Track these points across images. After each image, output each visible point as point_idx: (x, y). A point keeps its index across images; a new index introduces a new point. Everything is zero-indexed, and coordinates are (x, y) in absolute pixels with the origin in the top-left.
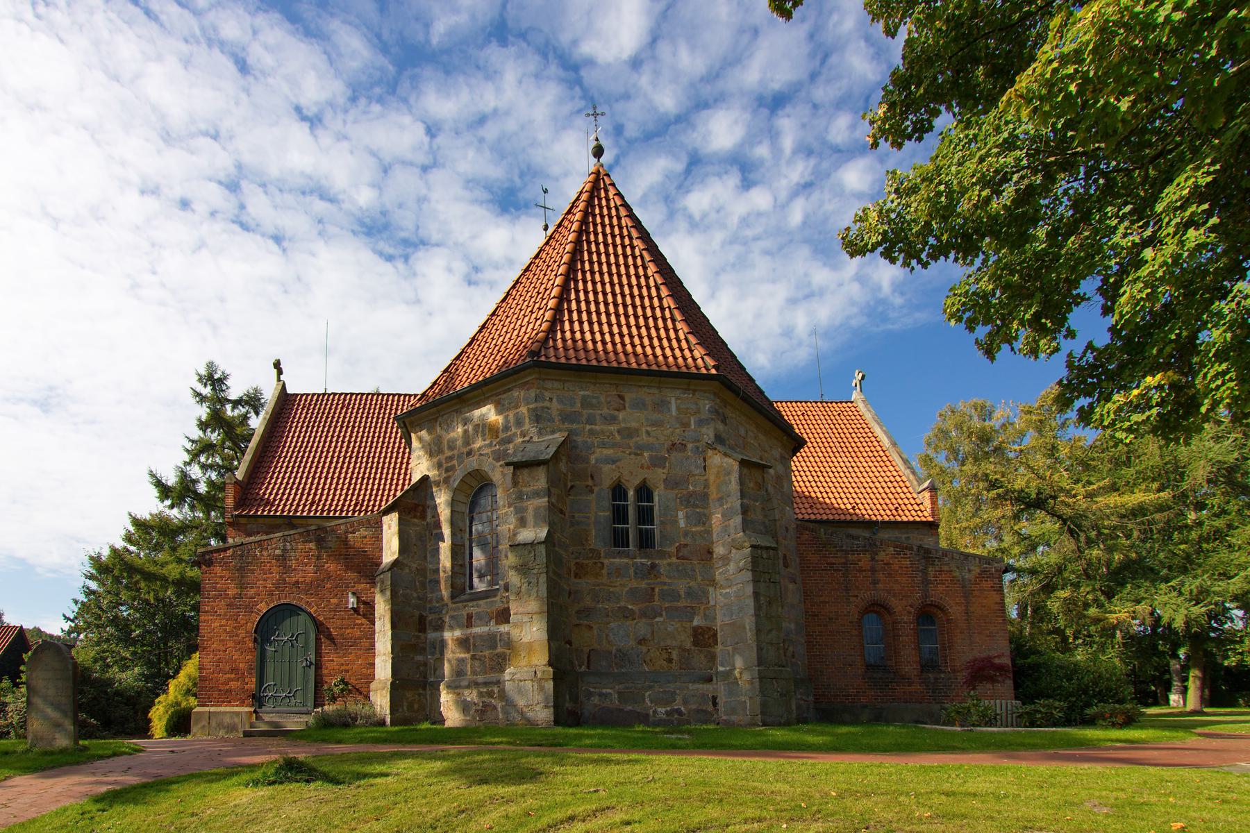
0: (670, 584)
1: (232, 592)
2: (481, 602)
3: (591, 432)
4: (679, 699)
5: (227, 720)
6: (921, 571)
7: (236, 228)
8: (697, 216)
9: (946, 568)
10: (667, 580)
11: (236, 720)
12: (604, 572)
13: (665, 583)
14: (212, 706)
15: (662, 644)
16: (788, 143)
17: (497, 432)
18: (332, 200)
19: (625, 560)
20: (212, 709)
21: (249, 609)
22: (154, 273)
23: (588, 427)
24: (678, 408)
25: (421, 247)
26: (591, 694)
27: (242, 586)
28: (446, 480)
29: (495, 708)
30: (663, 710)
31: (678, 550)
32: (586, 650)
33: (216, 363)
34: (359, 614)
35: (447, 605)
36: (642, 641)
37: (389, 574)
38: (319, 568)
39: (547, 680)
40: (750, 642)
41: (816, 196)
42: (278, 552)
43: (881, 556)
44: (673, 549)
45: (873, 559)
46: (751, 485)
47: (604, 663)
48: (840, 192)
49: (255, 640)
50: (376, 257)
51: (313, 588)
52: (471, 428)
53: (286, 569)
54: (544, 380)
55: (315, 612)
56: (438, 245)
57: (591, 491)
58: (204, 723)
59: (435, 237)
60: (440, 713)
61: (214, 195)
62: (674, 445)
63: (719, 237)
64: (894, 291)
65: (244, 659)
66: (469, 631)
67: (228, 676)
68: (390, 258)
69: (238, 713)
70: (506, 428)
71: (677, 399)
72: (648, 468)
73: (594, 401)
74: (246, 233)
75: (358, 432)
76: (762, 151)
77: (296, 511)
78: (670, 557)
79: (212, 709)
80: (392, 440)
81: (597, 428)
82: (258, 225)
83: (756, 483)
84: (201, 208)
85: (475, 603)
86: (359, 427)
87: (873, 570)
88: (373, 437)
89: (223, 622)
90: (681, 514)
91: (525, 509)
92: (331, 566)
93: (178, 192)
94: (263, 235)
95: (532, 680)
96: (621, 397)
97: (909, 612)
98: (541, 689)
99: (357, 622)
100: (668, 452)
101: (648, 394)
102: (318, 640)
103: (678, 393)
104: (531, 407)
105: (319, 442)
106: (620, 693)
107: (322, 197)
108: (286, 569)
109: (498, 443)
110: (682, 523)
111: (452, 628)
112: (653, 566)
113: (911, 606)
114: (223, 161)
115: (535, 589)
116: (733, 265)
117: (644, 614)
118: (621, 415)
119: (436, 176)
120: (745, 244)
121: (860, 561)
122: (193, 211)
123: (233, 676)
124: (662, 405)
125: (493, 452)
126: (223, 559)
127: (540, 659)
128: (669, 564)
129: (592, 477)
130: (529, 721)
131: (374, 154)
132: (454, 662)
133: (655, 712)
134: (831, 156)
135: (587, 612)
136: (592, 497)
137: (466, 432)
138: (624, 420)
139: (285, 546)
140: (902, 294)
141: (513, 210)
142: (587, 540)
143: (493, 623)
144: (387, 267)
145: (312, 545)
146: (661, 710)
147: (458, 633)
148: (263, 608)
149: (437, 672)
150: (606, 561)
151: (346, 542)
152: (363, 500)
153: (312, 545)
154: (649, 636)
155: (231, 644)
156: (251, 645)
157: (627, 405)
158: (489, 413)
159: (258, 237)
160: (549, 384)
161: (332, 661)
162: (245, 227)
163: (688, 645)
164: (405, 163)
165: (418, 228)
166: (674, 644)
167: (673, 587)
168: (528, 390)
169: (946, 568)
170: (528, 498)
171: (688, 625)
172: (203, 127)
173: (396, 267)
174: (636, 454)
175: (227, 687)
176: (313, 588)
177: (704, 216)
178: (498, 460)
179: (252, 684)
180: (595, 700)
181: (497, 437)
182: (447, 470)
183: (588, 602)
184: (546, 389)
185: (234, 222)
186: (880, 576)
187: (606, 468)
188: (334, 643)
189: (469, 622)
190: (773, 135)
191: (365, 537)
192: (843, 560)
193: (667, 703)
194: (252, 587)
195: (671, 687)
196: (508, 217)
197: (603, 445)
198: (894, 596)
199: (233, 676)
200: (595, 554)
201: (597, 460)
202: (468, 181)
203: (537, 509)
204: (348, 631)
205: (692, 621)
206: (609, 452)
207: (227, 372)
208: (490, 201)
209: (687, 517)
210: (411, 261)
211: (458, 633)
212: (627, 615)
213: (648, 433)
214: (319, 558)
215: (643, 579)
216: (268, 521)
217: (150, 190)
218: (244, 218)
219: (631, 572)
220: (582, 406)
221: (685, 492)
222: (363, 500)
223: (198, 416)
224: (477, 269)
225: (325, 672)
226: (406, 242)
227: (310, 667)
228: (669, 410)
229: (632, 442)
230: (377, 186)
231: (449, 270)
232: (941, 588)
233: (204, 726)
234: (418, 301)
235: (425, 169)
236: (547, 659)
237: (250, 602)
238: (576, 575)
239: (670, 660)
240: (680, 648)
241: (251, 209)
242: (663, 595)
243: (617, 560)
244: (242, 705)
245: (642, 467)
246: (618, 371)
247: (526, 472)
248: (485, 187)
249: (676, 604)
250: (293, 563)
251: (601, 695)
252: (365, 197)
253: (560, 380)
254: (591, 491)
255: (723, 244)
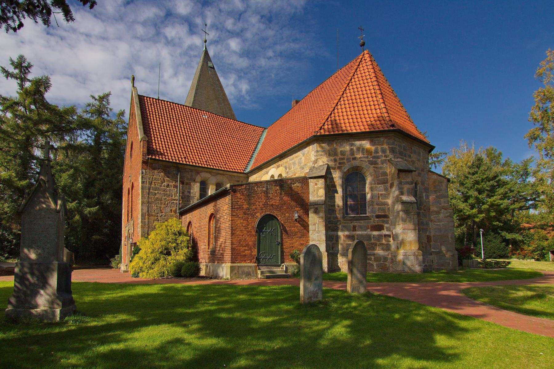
1: (245, 207)
2: (362, 221)
5: (246, 270)
8: (169, 39)
11: (250, 270)
14: (238, 263)
16: (209, 22)
17: (371, 152)
20: (239, 264)
21: (253, 216)
27: (249, 204)
28: (339, 168)
29: (373, 265)
33: (26, 57)
34: (297, 222)
35: (340, 221)
37: (324, 206)
38: (281, 199)
39: (420, 256)
40: (450, 242)
41: (219, 47)
42: (264, 189)
48: (228, 47)
49: (257, 232)
51: (279, 208)
52: (355, 148)
53: (268, 198)
55: (280, 219)
58: (236, 271)
60: (338, 266)
63: (179, 51)
64: (247, 94)
65: (252, 240)
66: (354, 233)
67: (244, 248)
69: (251, 267)
70: (376, 151)
76: (198, 21)
79: (239, 264)
85: (358, 221)
89: (242, 221)
91: (403, 188)
92: (285, 198)
95: (414, 256)
98: (417, 259)
99: (296, 225)
104: (390, 146)
108: (268, 198)
109: (372, 157)
111: (342, 231)
115: (413, 220)
116: (185, 65)
120: (190, 57)
123: (246, 248)
125: (368, 161)
126: (240, 190)
127: (415, 247)
130: (413, 271)
132: (345, 245)
134: (225, 33)
137: (352, 149)
139: (267, 187)
140: (250, 96)
143: (368, 230)
145: (278, 188)
147: (347, 233)
149: (334, 249)
151: (291, 188)
153: (278, 188)
155: (245, 232)
156: (254, 233)
158: (366, 144)
161: (287, 242)
168: (389, 139)
170: (404, 184)
175: (244, 254)
176: (279, 208)
177: (172, 40)
178: (371, 164)
179: (255, 252)
181: (371, 155)
182: (340, 163)
188: (287, 234)
189: (354, 229)
190: (203, 16)
191: (298, 187)
194: (254, 205)
199: (246, 248)
203: (408, 189)
204: (292, 229)
207: (32, 64)
211: (347, 233)
214: (281, 194)
216: (164, 163)
225: (284, 247)
227: (279, 245)
233: (236, 273)
236: (418, 247)
237: (253, 212)
244: (251, 262)
247: (403, 174)
250: (271, 195)
253: (399, 138)
255: (180, 55)
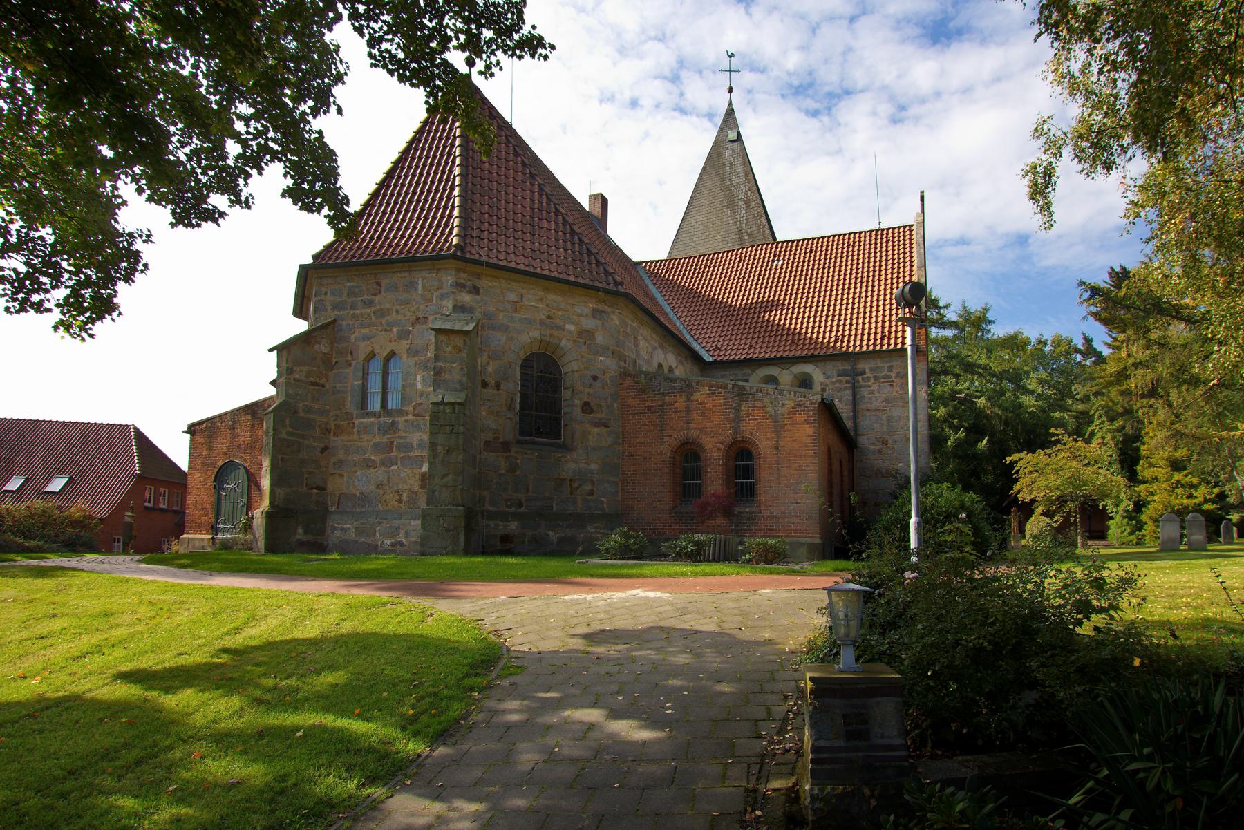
0: (406, 437)
3: (354, 316)
4: (402, 533)
6: (734, 408)
7: (676, 114)
9: (759, 404)
10: (404, 434)
12: (355, 430)
13: (401, 437)
15: (395, 488)
18: (763, 71)
19: (372, 420)
20: (191, 536)
21: (214, 464)
22: (608, 169)
23: (352, 312)
24: (424, 287)
25: (845, 97)
26: (335, 528)
27: (210, 449)
30: (389, 542)
31: (414, 409)
32: (338, 494)
36: (379, 486)
43: (697, 396)
44: (411, 409)
45: (688, 400)
46: (449, 349)
47: (350, 504)
49: (215, 487)
50: (802, 116)
54: (321, 278)
56: (862, 91)
57: (350, 365)
59: (860, 85)
61: (657, 90)
62: (418, 319)
68: (815, 114)
69: (203, 539)
71: (424, 278)
72: (395, 341)
73: (357, 290)
74: (685, 118)
75: (823, 273)
77: (875, 345)
78: (407, 415)
79: (191, 536)
80: (819, 280)
81: (358, 312)
82: (694, 108)
83: (455, 347)
84: (646, 102)
86: (835, 267)
87: (688, 410)
88: (788, 285)
90: (419, 378)
93: (627, 95)
94: (698, 116)
96: (379, 284)
97: (719, 449)
100: (413, 325)
101: (400, 278)
102: (249, 486)
103: (424, 274)
105: (781, 291)
106: (356, 528)
107: (752, 70)
110: (419, 386)
112: (393, 423)
113: (722, 443)
114: (662, 56)
117: (383, 464)
118: (377, 299)
119: (864, 23)
121: (676, 402)
122: (642, 106)
124: (411, 285)
128: (406, 421)
129: (351, 353)
131: (802, 17)
133: (383, 543)
135: (340, 463)
136: (350, 370)
138: (379, 303)
141: (943, 39)
142: (344, 405)
144: (813, 123)
146: (388, 542)
148: (220, 463)
150: (357, 422)
152: (843, 336)
154: (385, 482)
157: (383, 290)
159: (694, 119)
160: (325, 281)
162: (682, 111)
163: (416, 488)
164: (831, 18)
165: (842, 80)
166: (406, 487)
167: (408, 440)
169: (759, 404)
171: (417, 471)
172: (653, 34)
173: (821, 121)
174: (386, 330)
180: (338, 533)
183: (341, 455)
184: (323, 285)
185: (675, 110)
186: (694, 415)
187: (363, 345)
192: (660, 403)
193: (392, 536)
195: (396, 523)
196: (938, 46)
197: (362, 326)
198: (706, 434)
200: (349, 416)
201: (356, 339)
202: (898, 22)
205: (421, 468)
206: (366, 331)
208: (923, 36)
209: (424, 380)
210: (834, 110)
212: (369, 464)
213: (397, 311)
215: (384, 434)
217: (607, 98)
218: (682, 104)
219: (376, 429)
220: (348, 295)
221: (423, 358)
222: (843, 336)
223: (65, 342)
224: (902, 108)
226: (831, 95)
228: (416, 289)
229: (384, 321)
230: (804, 48)
231: (874, 113)
232: (752, 423)
234: (840, 151)
235: (852, 19)
238: (335, 434)
239: (400, 501)
240: (410, 490)
241: (689, 96)
242: (399, 447)
243: (365, 420)
244: (207, 534)
245: (390, 341)
246: (375, 263)
248: (916, 24)
249: (412, 454)
251: (342, 529)
252: (793, 61)
254: (350, 365)
